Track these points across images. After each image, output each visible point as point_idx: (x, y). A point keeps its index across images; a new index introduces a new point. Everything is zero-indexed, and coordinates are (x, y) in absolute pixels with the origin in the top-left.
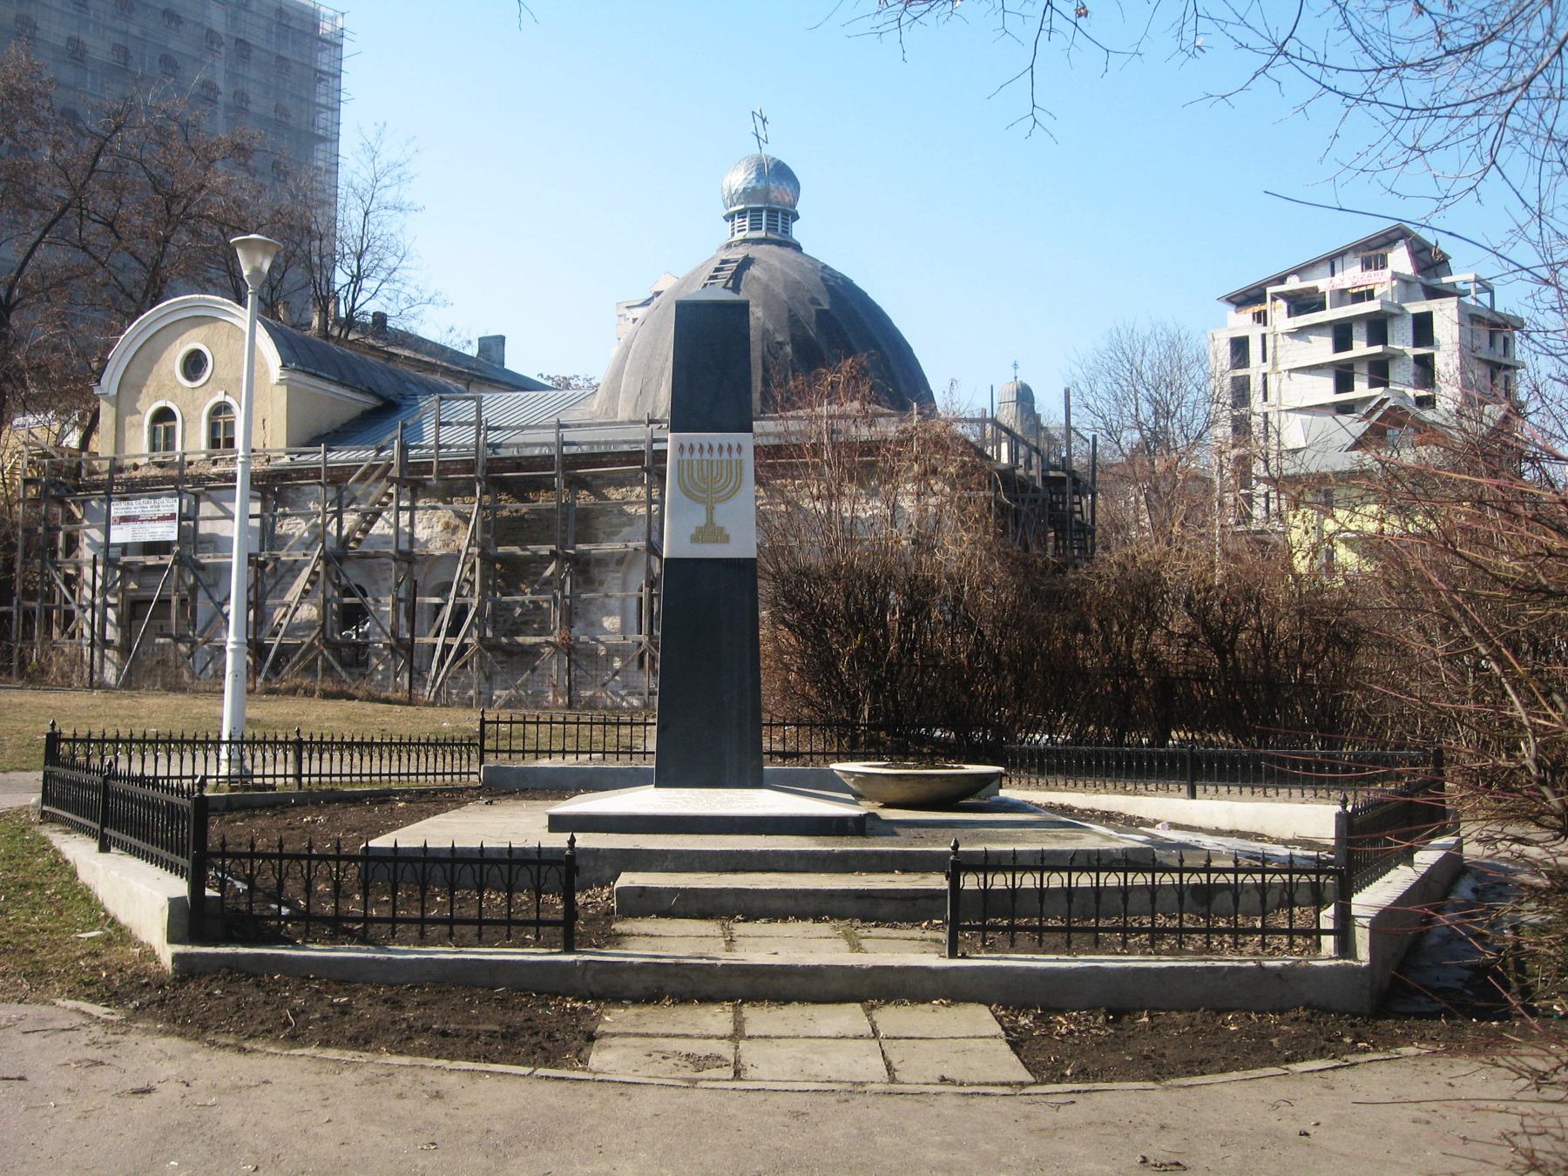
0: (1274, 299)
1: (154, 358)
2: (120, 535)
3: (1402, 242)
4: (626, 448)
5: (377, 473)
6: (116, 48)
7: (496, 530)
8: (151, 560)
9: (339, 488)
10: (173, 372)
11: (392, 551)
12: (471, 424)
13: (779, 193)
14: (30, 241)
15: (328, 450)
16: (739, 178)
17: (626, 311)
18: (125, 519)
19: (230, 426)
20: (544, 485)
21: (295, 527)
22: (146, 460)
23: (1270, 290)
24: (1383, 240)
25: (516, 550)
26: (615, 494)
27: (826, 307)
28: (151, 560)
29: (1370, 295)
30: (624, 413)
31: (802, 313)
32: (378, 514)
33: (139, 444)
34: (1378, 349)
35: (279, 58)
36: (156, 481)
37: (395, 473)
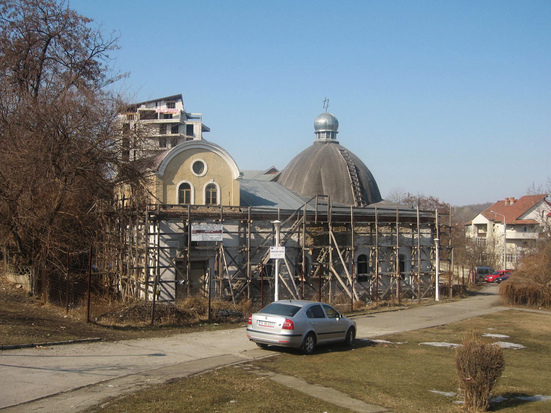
1: (181, 163)
18: (199, 232)
19: (215, 194)
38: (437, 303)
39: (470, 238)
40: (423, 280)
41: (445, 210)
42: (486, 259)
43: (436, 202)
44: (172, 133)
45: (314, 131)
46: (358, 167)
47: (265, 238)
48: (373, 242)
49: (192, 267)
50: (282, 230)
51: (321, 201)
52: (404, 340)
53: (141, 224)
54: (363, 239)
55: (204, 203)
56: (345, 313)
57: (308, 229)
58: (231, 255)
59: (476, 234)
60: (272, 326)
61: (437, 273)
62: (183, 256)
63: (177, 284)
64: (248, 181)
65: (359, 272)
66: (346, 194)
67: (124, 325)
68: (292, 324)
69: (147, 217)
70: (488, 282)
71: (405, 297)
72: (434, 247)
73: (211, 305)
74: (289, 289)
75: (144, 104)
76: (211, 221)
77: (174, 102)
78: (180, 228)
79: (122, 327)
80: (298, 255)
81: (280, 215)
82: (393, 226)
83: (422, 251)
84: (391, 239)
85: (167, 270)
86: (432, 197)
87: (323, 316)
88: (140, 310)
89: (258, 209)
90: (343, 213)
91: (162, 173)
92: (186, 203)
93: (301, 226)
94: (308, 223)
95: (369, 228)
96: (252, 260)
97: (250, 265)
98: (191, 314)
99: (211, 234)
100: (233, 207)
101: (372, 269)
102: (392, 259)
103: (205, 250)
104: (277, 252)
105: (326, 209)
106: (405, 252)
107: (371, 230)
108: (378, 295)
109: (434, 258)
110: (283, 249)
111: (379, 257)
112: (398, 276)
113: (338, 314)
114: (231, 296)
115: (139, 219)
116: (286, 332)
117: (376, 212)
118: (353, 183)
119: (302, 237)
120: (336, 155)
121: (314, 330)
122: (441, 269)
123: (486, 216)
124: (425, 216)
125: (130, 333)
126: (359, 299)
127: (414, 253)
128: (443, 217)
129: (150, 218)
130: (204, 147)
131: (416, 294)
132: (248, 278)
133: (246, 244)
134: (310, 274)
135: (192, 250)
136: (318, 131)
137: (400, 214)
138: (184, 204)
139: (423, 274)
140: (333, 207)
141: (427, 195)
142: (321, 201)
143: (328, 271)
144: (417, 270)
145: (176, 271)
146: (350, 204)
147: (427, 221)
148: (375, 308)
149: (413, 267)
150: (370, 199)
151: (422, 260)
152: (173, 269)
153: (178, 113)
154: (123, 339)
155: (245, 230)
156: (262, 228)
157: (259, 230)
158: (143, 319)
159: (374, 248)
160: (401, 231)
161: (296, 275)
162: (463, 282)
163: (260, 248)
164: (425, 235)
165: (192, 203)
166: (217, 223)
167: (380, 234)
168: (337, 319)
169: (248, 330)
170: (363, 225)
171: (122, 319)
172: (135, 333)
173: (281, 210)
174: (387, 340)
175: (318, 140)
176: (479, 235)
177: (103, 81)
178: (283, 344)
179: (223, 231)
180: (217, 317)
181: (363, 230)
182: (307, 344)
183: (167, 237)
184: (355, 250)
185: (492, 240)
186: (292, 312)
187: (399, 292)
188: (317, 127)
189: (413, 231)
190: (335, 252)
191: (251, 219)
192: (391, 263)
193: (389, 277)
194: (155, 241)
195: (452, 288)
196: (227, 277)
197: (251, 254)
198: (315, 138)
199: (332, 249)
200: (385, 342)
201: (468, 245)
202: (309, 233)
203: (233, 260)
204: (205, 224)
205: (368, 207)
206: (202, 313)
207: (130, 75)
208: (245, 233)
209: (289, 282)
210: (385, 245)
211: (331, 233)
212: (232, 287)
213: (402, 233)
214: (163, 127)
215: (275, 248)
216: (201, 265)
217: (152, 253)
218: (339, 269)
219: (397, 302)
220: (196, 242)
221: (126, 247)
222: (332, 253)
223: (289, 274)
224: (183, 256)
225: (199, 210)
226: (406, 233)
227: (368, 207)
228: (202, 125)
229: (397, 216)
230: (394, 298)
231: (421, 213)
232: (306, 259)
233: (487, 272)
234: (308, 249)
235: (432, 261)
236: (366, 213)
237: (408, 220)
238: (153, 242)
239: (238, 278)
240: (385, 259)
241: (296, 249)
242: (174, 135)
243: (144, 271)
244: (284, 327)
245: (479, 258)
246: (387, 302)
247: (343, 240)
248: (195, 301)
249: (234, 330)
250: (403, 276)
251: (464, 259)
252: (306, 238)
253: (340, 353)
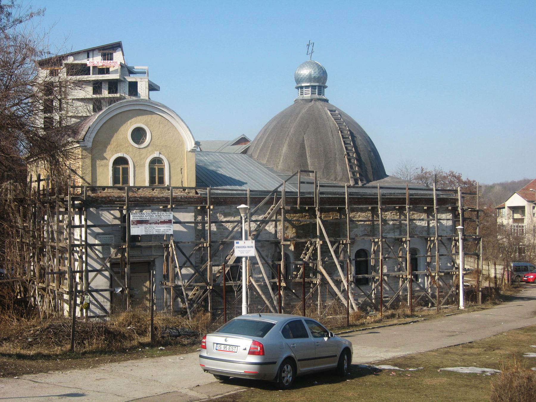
19: (161, 171)
38: (462, 312)
39: (503, 225)
40: (443, 281)
41: (470, 190)
42: (524, 253)
43: (459, 178)
44: (109, 93)
45: (295, 85)
46: (354, 133)
47: (230, 229)
48: (376, 232)
49: (132, 270)
50: (254, 218)
51: (305, 178)
52: (419, 365)
53: (63, 213)
54: (362, 229)
55: (147, 184)
56: (339, 328)
57: (288, 216)
58: (185, 253)
59: (511, 221)
60: (235, 351)
61: (461, 272)
62: (119, 256)
63: (112, 293)
64: (207, 153)
65: (358, 272)
66: (338, 168)
67: (32, 353)
68: (262, 348)
69: (70, 203)
70: (528, 282)
71: (420, 304)
72: (457, 238)
73: (154, 322)
74: (263, 297)
75: (72, 54)
76: (157, 207)
77: (111, 52)
78: (116, 218)
79: (29, 356)
80: (275, 251)
81: (251, 198)
82: (401, 210)
83: (441, 242)
84: (400, 228)
85: (99, 275)
86: (452, 173)
87: (306, 336)
88: (55, 332)
89: (220, 190)
90: (335, 193)
91: (89, 145)
92: (123, 183)
93: (278, 212)
94: (288, 208)
95: (369, 214)
96: (213, 259)
97: (211, 266)
98: (127, 335)
99: (157, 225)
100: (187, 188)
101: (374, 268)
102: (400, 255)
103: (150, 247)
104: (244, 247)
105: (311, 188)
106: (418, 245)
107: (373, 216)
108: (383, 303)
109: (457, 253)
110: (251, 243)
111: (384, 252)
112: (409, 277)
113: (326, 331)
114: (185, 308)
115: (60, 207)
116: (255, 359)
117: (379, 192)
118: (348, 154)
119: (280, 227)
120: (325, 117)
121: (293, 354)
122: (466, 267)
123: (524, 196)
124: (444, 197)
125: (40, 363)
126: (358, 308)
127: (430, 246)
128: (468, 197)
129: (73, 206)
130: (147, 109)
131: (434, 301)
132: (208, 284)
133: (205, 238)
134: (292, 277)
135: (132, 247)
136: (299, 85)
137: (411, 195)
138: (120, 185)
139: (443, 274)
140: (321, 186)
141: (446, 170)
142: (305, 178)
143: (316, 272)
144: (435, 269)
145: (111, 275)
146: (345, 183)
147: (446, 203)
148: (380, 321)
149: (429, 264)
150: (370, 176)
151: (440, 255)
152: (107, 273)
153: (118, 67)
154: (28, 373)
155: (203, 218)
156: (225, 216)
157: (222, 218)
158: (59, 343)
159: (376, 240)
160: (413, 217)
161: (273, 278)
162: (496, 283)
163: (223, 243)
164: (444, 222)
165: (131, 184)
166: (165, 211)
167: (385, 221)
168: (326, 339)
169: (201, 356)
170: (362, 210)
171: (31, 344)
172: (46, 363)
173: (251, 191)
174: (395, 365)
175: (301, 97)
176: (515, 220)
177: (8, 21)
178: (250, 376)
179: (173, 221)
180: (163, 337)
181: (362, 217)
182: (283, 375)
183: (97, 230)
184: (353, 242)
185: (532, 227)
186: (261, 330)
187: (412, 298)
188: (298, 80)
189: (428, 217)
190: (324, 246)
191: (211, 203)
192: (400, 259)
193: (397, 278)
194: (81, 236)
195: (482, 291)
196: (180, 283)
197: (212, 252)
198: (296, 95)
199: (321, 242)
200: (392, 368)
201: (500, 235)
202: (290, 221)
203: (188, 259)
204: (149, 211)
205: (368, 185)
206: (142, 333)
207: (46, 13)
208: (204, 223)
209: (264, 287)
210: (391, 235)
211: (318, 221)
212: (187, 295)
213: (414, 220)
214: (97, 86)
215: (241, 243)
216: (144, 267)
217: (78, 252)
218: (331, 269)
219: (408, 312)
220: (138, 236)
221: (44, 246)
222: (321, 248)
223: (263, 277)
224: (119, 256)
225: (142, 193)
226: (420, 220)
227: (368, 185)
228: (149, 81)
229: (407, 197)
230: (404, 306)
231: (438, 193)
232: (287, 256)
233: (526, 269)
234: (289, 243)
235: (454, 256)
236: (365, 194)
237: (421, 203)
238: (79, 238)
239: (195, 284)
240: (391, 255)
241: (272, 243)
242: (111, 95)
243: (67, 276)
244: (251, 353)
245: (516, 250)
246: (395, 312)
247: (336, 230)
248: (134, 316)
249: (185, 356)
250: (416, 277)
251: (496, 252)
252: (285, 228)
253: (330, 385)
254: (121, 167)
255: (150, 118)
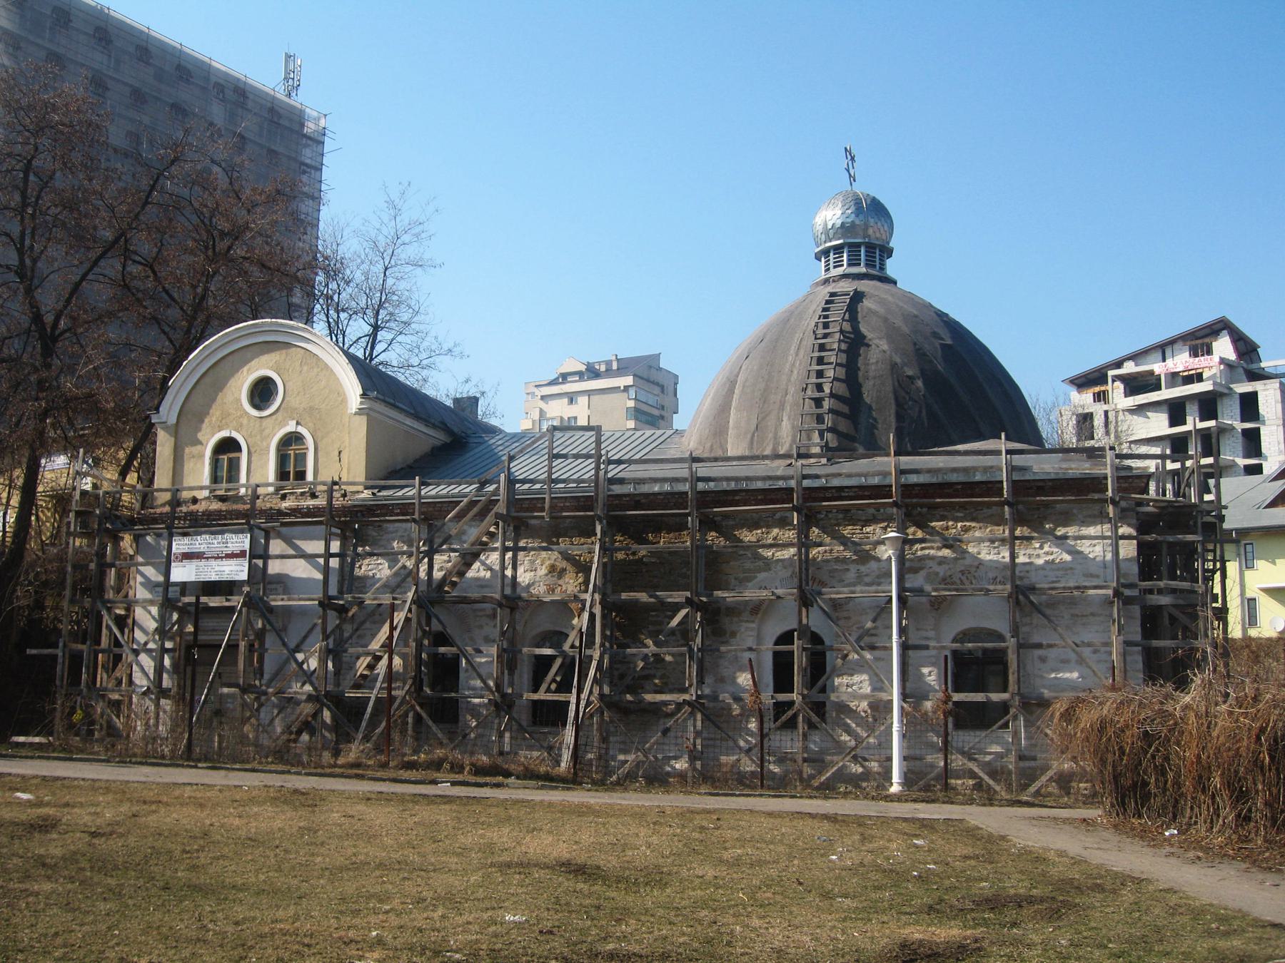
0: (1113, 381)
1: (220, 386)
2: (181, 573)
3: (1225, 332)
4: (759, 485)
5: (475, 510)
6: (129, 134)
7: (618, 575)
8: (215, 602)
9: (430, 526)
10: (239, 400)
11: (497, 596)
12: (587, 456)
13: (875, 232)
14: (92, 256)
15: (422, 484)
16: (832, 215)
17: (535, 390)
18: (188, 556)
19: (301, 458)
20: (678, 526)
21: (377, 569)
22: (206, 493)
23: (1111, 373)
24: (1208, 331)
25: (643, 597)
26: (748, 536)
27: (949, 342)
28: (215, 602)
29: (1199, 377)
30: (734, 448)
31: (927, 347)
32: (476, 556)
33: (199, 474)
34: (1212, 423)
35: (272, 152)
36: (218, 515)
37: (501, 508)
99: (219, 562)
174: (934, 910)
214: (1176, 411)
254: (225, 457)
255: (284, 356)
